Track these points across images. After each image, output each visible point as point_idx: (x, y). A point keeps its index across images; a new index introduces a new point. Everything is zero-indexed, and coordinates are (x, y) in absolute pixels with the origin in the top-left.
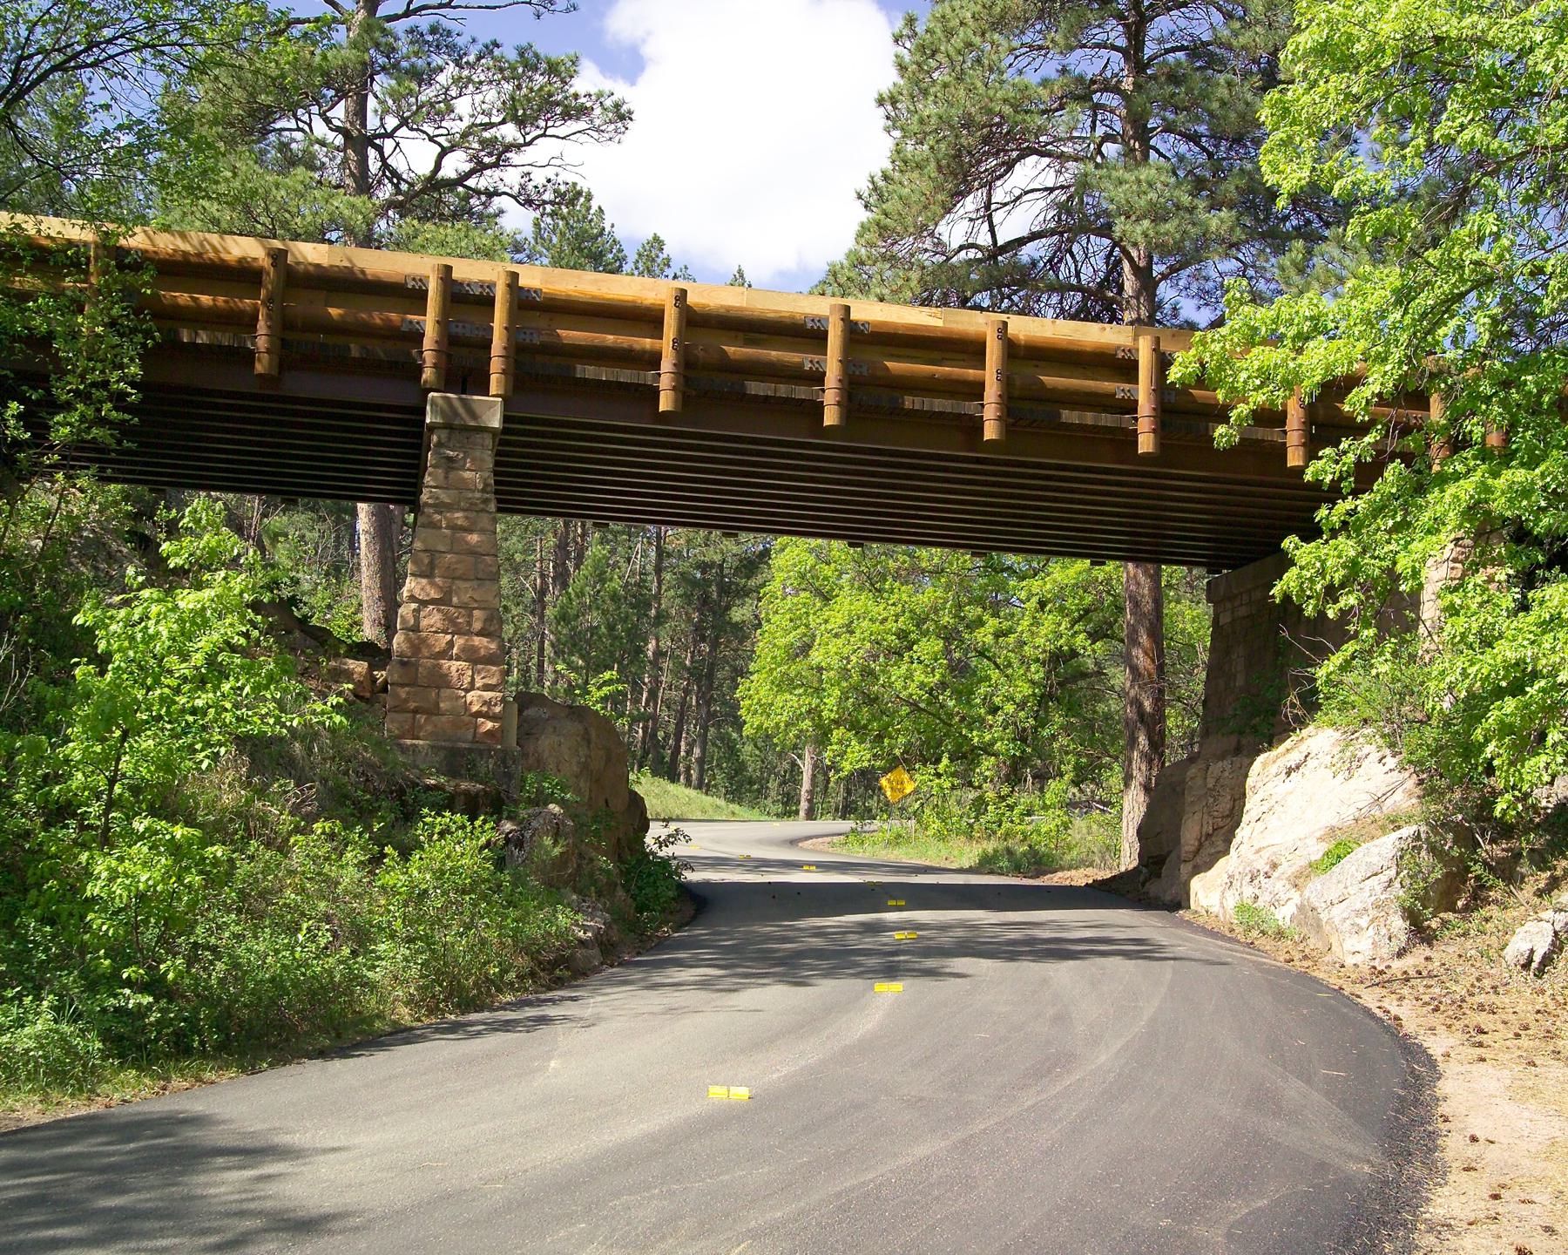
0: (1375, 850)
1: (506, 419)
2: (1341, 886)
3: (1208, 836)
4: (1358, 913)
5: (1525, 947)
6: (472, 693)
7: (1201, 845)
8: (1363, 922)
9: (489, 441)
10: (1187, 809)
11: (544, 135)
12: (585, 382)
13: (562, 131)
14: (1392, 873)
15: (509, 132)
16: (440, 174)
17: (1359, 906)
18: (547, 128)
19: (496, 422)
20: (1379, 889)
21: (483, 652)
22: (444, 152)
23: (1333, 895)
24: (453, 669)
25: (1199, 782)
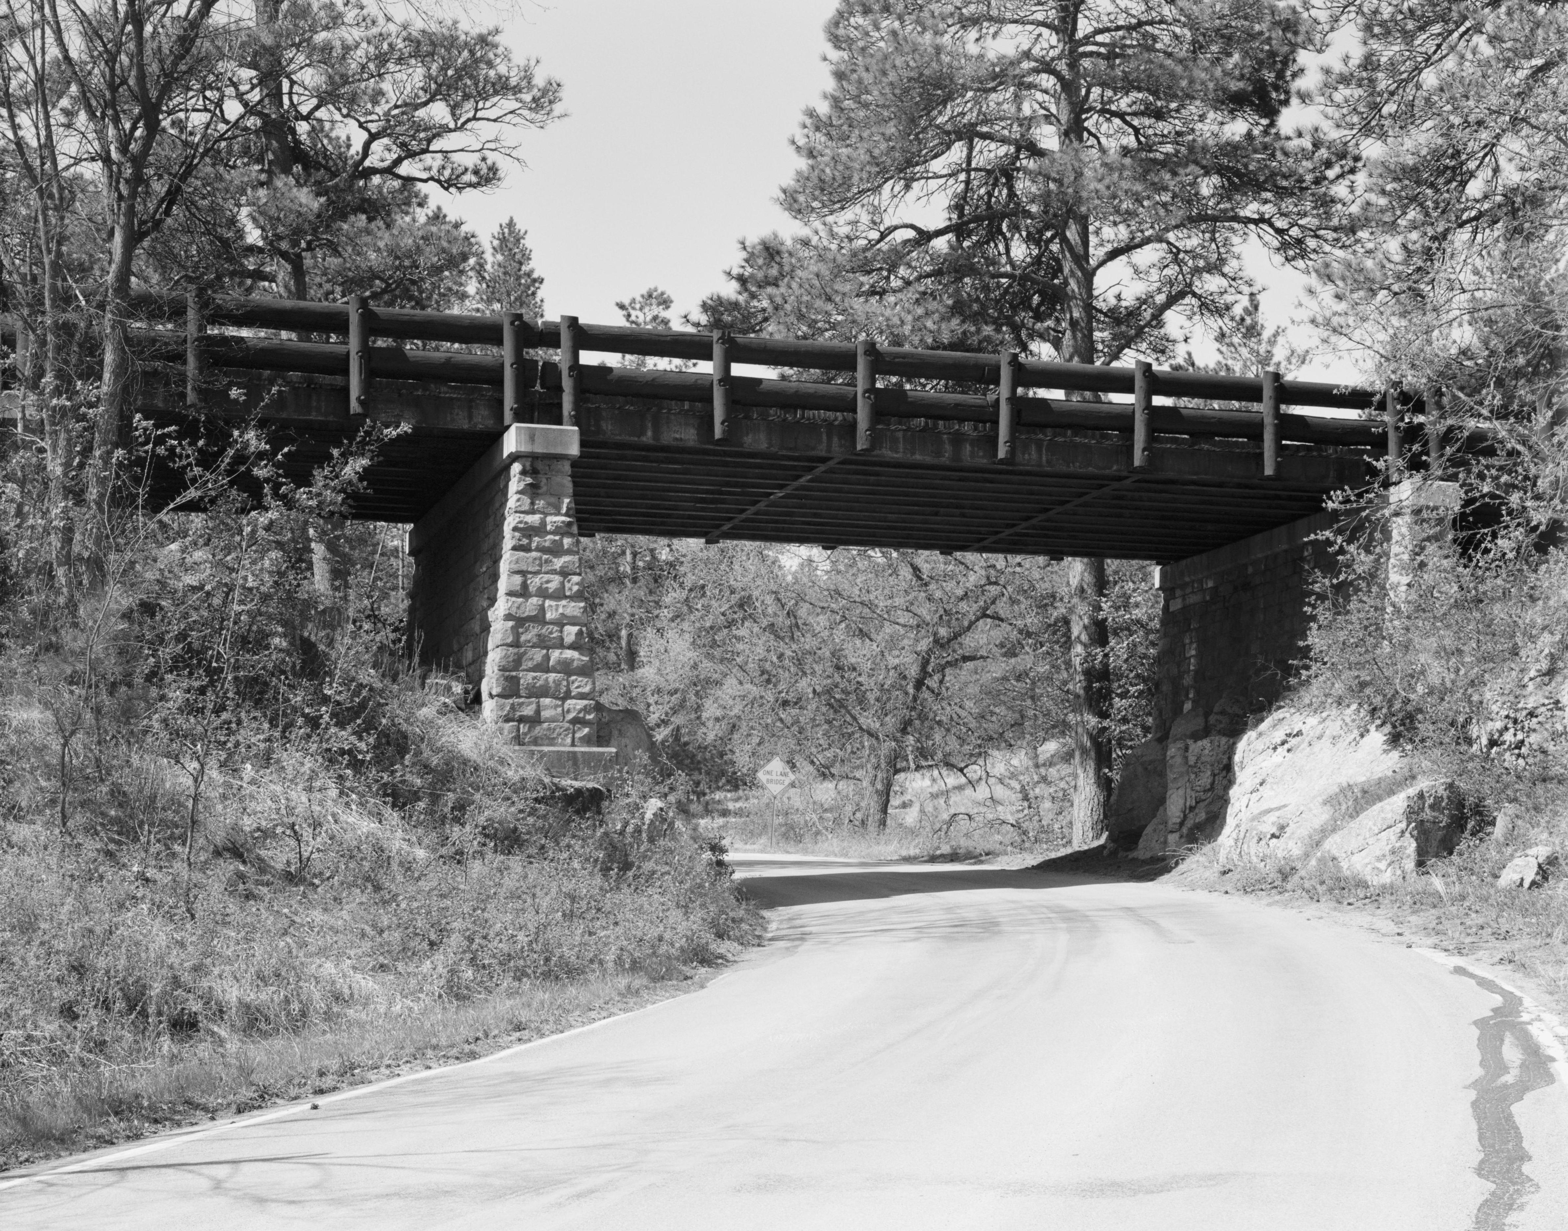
0: (1388, 808)
1: (583, 444)
2: (1360, 838)
3: (1192, 809)
4: (1379, 859)
5: (1516, 877)
6: (569, 701)
7: (1185, 817)
8: (1382, 865)
9: (567, 467)
10: (1170, 785)
11: (474, 118)
12: (289, 328)
13: (492, 114)
14: (1403, 825)
15: (439, 112)
16: (367, 163)
17: (1378, 853)
18: (476, 110)
19: (574, 450)
20: (1393, 838)
21: (575, 664)
22: (373, 137)
23: (1354, 844)
24: (551, 680)
25: (1179, 760)
